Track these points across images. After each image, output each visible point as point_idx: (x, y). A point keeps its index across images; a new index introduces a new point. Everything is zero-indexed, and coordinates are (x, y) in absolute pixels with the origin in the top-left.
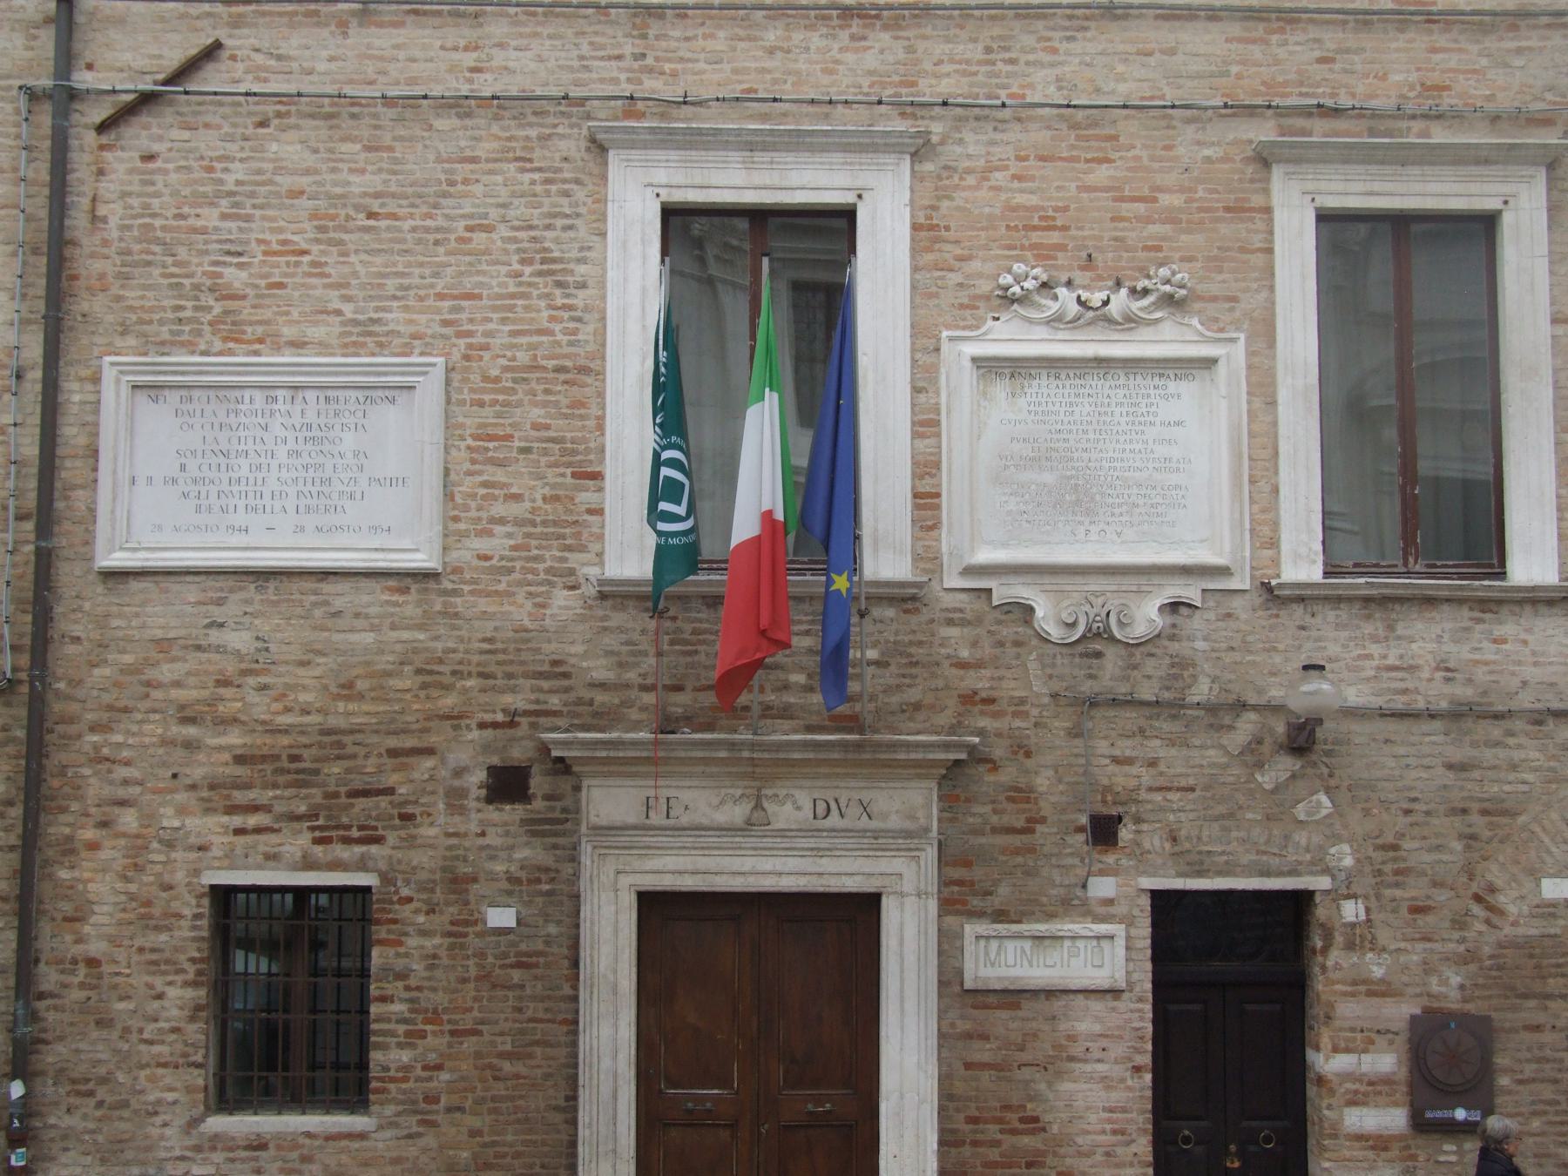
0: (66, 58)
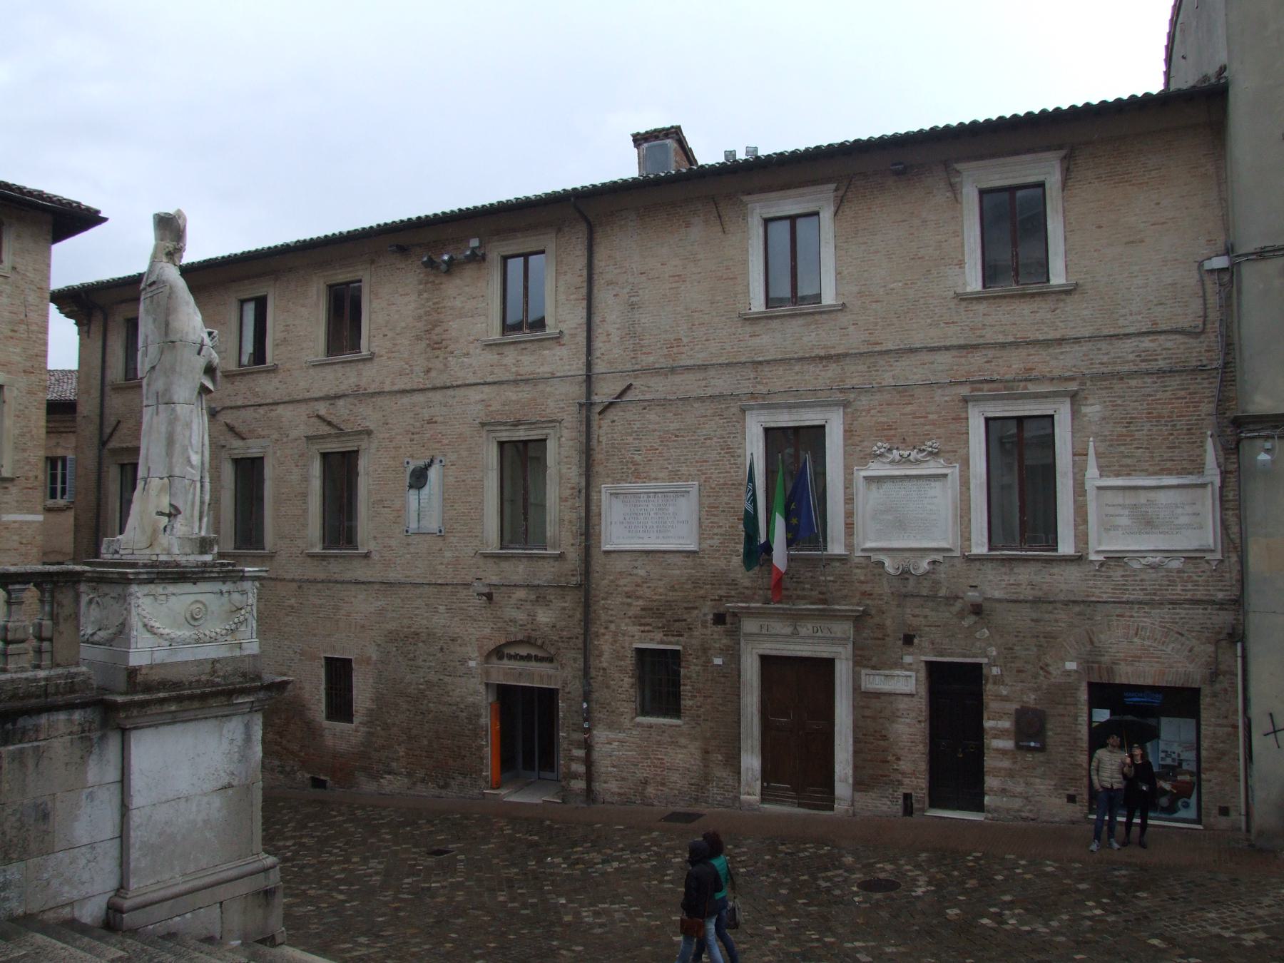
0: (589, 392)
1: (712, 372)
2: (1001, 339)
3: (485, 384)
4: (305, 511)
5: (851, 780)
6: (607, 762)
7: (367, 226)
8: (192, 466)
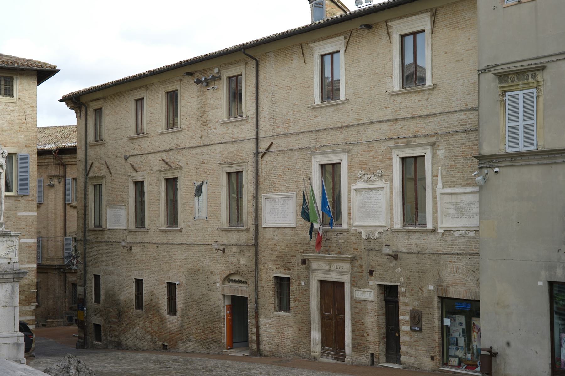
1: (301, 136)
2: (406, 115)
3: (221, 143)
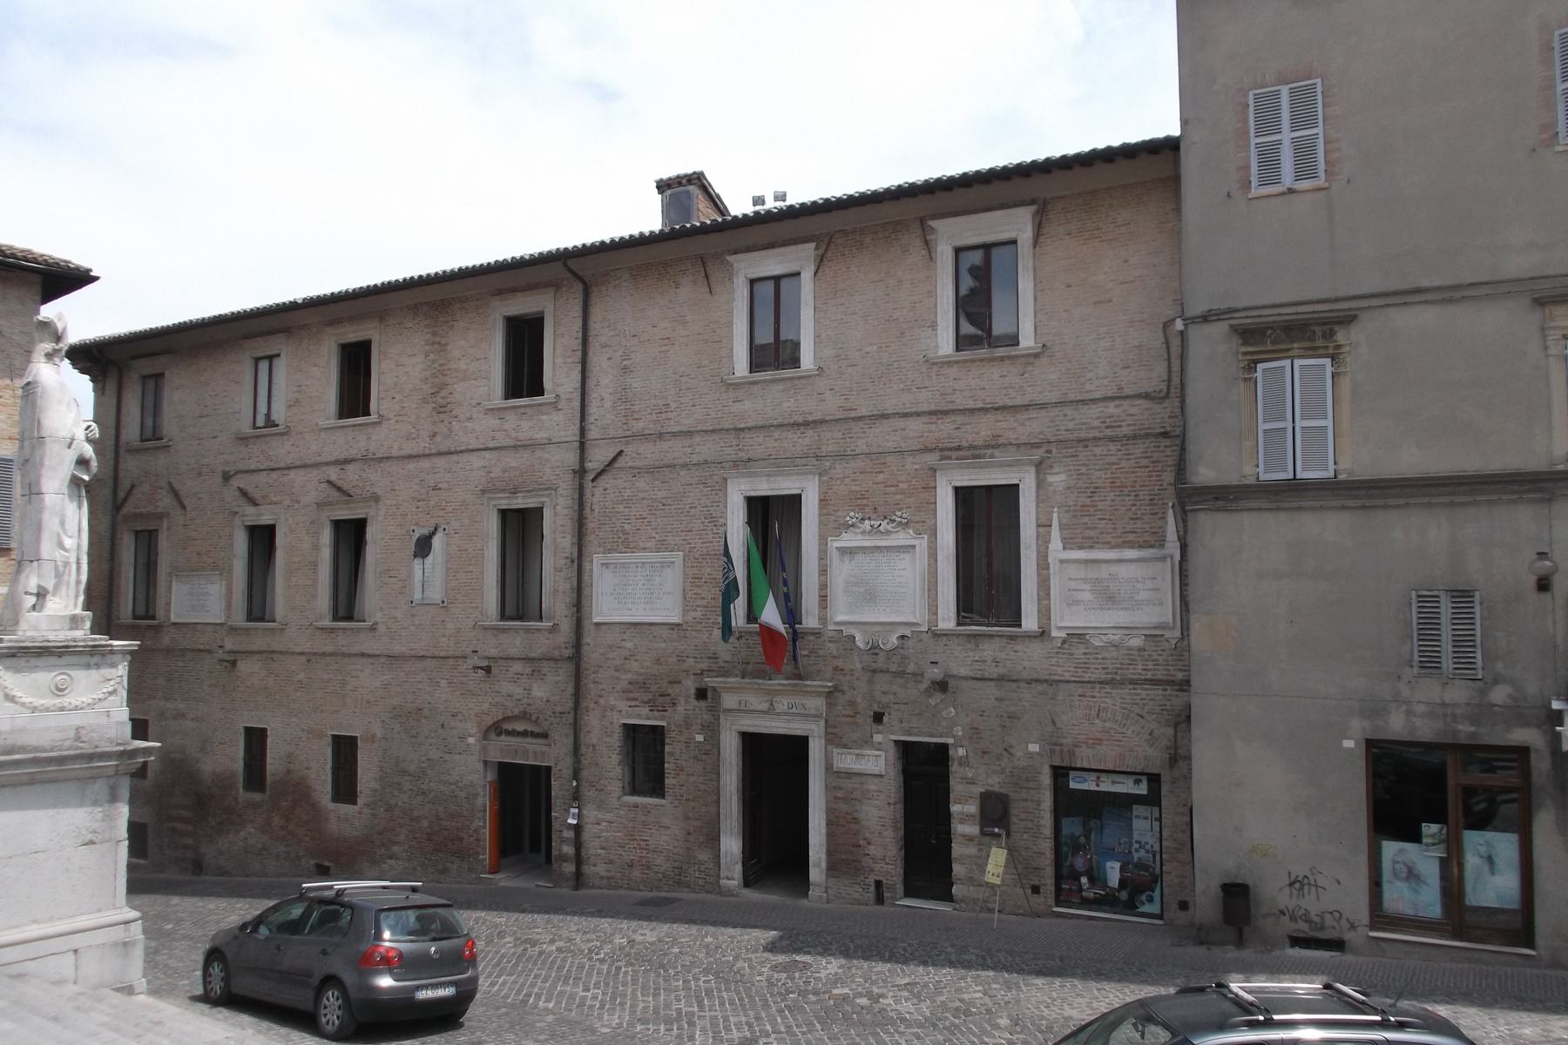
0: (582, 459)
1: (697, 439)
2: (970, 404)
3: (486, 449)
4: (315, 581)
5: (824, 865)
6: (596, 843)
7: (372, 283)
8: (66, 550)
